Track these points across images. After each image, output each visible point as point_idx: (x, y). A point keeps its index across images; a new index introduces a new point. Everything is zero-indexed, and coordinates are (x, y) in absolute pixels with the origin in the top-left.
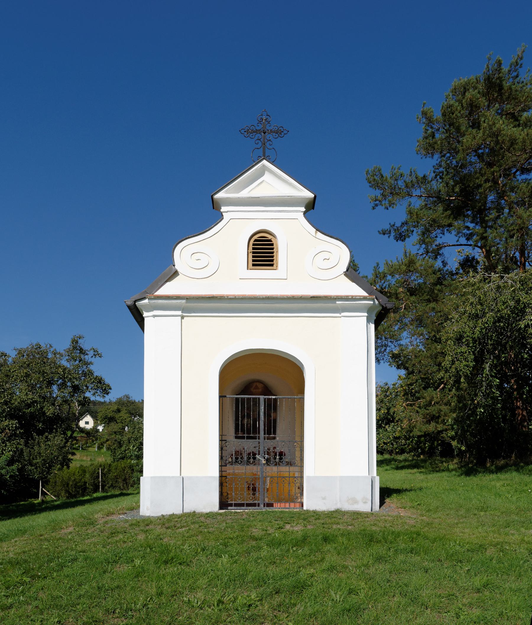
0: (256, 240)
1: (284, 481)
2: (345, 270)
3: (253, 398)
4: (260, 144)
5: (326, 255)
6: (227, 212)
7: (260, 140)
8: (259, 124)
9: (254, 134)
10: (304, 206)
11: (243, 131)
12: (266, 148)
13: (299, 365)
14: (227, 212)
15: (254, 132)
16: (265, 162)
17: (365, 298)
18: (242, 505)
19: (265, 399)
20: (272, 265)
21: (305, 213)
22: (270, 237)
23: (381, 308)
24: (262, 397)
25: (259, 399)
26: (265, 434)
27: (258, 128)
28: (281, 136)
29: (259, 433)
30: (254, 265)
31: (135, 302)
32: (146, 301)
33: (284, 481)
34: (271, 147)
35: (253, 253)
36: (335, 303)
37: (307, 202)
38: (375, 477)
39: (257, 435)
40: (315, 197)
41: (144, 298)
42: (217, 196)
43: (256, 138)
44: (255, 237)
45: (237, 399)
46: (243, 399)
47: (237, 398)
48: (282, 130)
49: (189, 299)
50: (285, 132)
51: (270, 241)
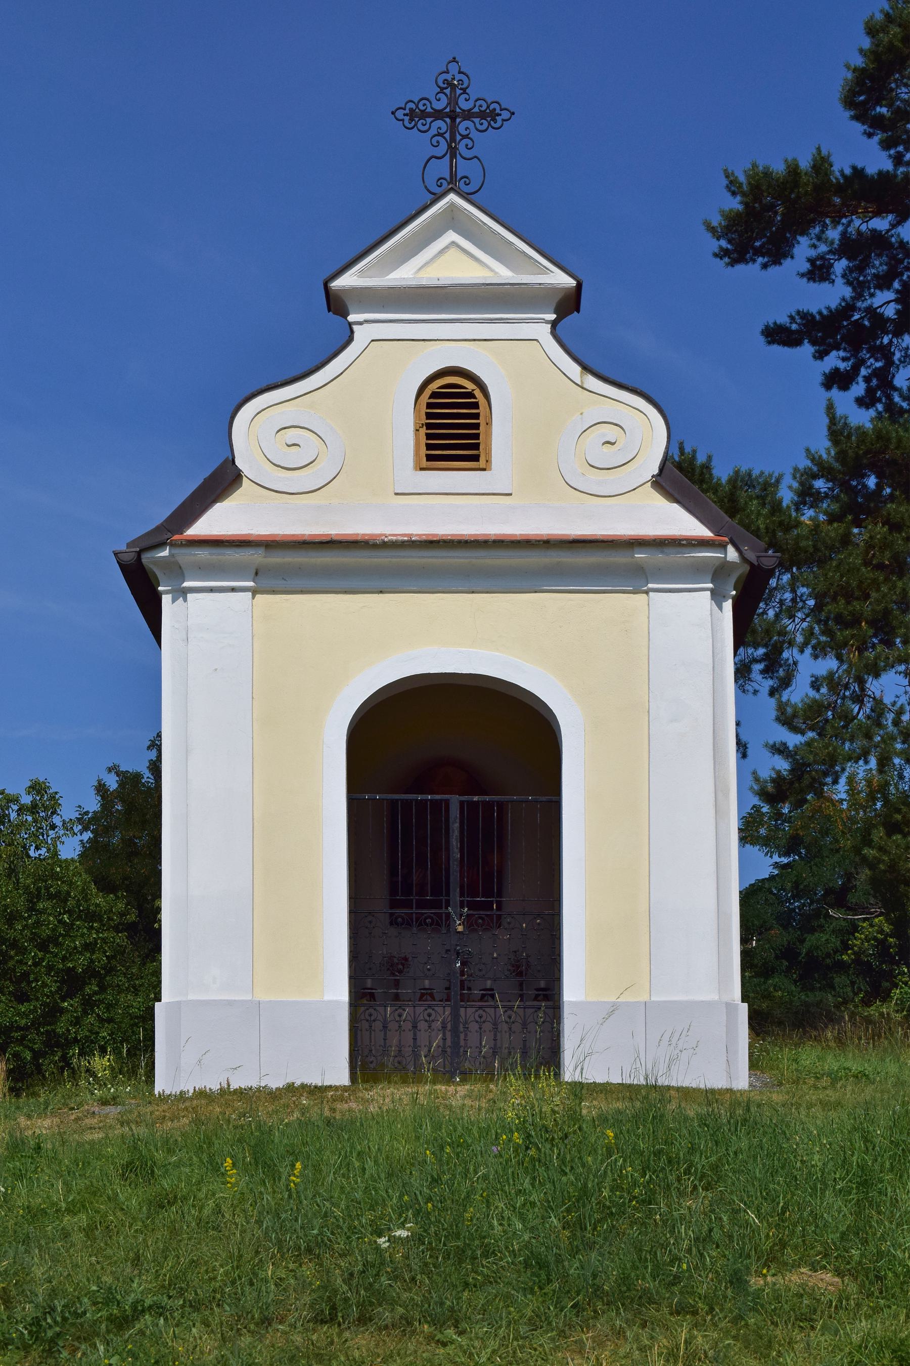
0: (434, 395)
1: (370, 922)
2: (656, 471)
3: (402, 800)
4: (444, 146)
5: (611, 433)
6: (360, 323)
7: (441, 135)
8: (441, 96)
9: (429, 120)
10: (553, 307)
11: (400, 114)
12: (449, 180)
13: (546, 716)
14: (360, 323)
15: (429, 115)
16: (452, 197)
17: (702, 543)
18: (370, 1037)
19: (462, 803)
20: (476, 458)
21: (554, 324)
22: (470, 386)
23: (747, 568)
24: (455, 800)
25: (447, 802)
26: (462, 895)
27: (439, 106)
28: (495, 125)
29: (448, 894)
30: (429, 458)
31: (139, 554)
32: (165, 553)
33: (370, 922)
34: (468, 154)
35: (429, 426)
36: (633, 557)
37: (560, 296)
38: (738, 1004)
39: (444, 898)
40: (579, 286)
41: (161, 545)
42: (339, 283)
43: (433, 131)
44: (434, 386)
45: (393, 803)
46: (407, 804)
47: (407, 800)
48: (498, 111)
49: (270, 544)
50: (505, 115)
51: (471, 395)
